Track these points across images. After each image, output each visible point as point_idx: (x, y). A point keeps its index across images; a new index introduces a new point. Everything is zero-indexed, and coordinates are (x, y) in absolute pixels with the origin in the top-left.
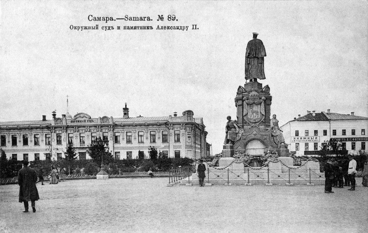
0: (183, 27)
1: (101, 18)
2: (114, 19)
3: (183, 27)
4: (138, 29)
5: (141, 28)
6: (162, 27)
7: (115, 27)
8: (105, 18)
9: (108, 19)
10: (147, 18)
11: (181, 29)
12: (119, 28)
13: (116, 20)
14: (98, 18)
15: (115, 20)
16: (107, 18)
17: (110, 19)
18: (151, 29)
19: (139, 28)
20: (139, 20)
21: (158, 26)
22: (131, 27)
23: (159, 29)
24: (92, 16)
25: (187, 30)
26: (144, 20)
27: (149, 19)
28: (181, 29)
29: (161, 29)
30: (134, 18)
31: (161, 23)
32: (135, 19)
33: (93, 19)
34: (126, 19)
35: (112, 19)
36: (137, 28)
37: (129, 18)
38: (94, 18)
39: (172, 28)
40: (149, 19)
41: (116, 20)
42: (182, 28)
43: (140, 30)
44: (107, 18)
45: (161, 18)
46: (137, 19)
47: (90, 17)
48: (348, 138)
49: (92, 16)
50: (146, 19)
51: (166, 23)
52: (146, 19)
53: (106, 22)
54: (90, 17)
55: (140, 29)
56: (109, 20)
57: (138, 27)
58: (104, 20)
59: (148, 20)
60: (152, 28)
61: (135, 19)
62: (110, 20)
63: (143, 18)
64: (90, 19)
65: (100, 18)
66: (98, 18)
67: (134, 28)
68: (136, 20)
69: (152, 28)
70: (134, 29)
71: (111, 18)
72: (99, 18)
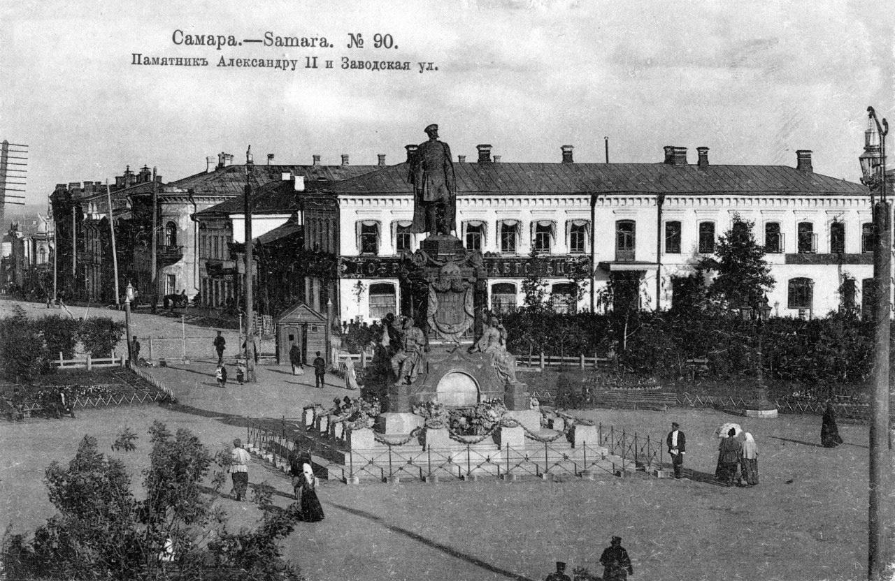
0: (284, 61)
1: (206, 39)
2: (238, 40)
3: (284, 61)
4: (172, 64)
5: (390, 66)
6: (232, 60)
7: (301, 63)
8: (216, 39)
9: (222, 41)
10: (319, 41)
11: (279, 66)
12: (329, 65)
13: (243, 43)
14: (197, 37)
15: (240, 44)
16: (219, 37)
17: (227, 40)
18: (203, 65)
19: (175, 62)
20: (300, 44)
21: (222, 58)
22: (153, 59)
23: (224, 65)
24: (182, 32)
25: (293, 69)
26: (313, 46)
27: (324, 43)
28: (279, 66)
29: (427, 69)
30: (287, 39)
31: (356, 54)
32: (289, 43)
33: (185, 39)
34: (268, 42)
35: (232, 42)
36: (169, 62)
37: (275, 41)
38: (187, 37)
39: (255, 63)
40: (324, 43)
41: (243, 43)
42: (282, 64)
43: (175, 67)
44: (219, 37)
45: (357, 40)
46: (295, 43)
47: (178, 34)
48: (232, 234)
49: (182, 32)
50: (317, 43)
51: (369, 52)
52: (317, 43)
53: (219, 48)
54: (178, 34)
55: (177, 64)
56: (224, 43)
57: (171, 59)
58: (213, 44)
59: (323, 44)
60: (205, 63)
61: (289, 43)
62: (302, 45)
63: (310, 41)
64: (178, 40)
65: (203, 37)
66: (197, 37)
67: (160, 61)
68: (292, 45)
69: (205, 63)
70: (162, 64)
71: (229, 38)
72: (200, 37)
